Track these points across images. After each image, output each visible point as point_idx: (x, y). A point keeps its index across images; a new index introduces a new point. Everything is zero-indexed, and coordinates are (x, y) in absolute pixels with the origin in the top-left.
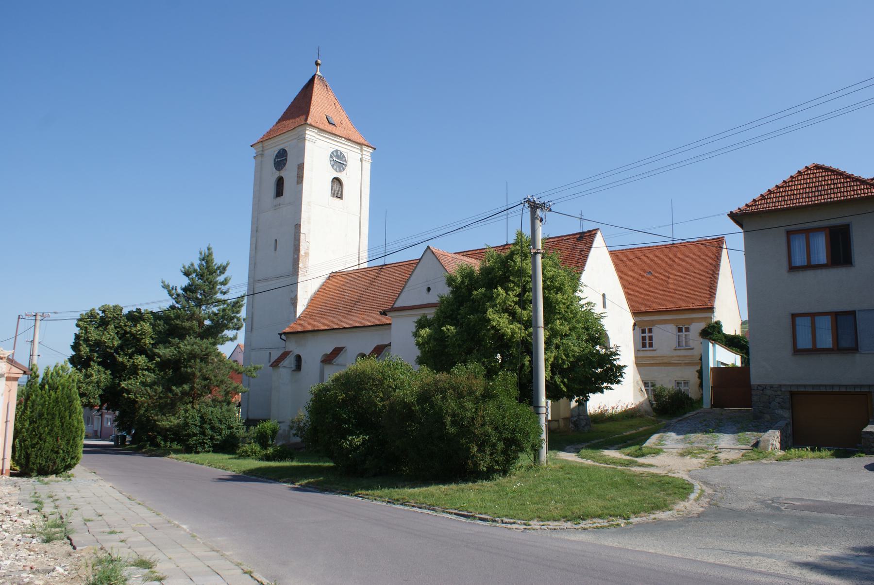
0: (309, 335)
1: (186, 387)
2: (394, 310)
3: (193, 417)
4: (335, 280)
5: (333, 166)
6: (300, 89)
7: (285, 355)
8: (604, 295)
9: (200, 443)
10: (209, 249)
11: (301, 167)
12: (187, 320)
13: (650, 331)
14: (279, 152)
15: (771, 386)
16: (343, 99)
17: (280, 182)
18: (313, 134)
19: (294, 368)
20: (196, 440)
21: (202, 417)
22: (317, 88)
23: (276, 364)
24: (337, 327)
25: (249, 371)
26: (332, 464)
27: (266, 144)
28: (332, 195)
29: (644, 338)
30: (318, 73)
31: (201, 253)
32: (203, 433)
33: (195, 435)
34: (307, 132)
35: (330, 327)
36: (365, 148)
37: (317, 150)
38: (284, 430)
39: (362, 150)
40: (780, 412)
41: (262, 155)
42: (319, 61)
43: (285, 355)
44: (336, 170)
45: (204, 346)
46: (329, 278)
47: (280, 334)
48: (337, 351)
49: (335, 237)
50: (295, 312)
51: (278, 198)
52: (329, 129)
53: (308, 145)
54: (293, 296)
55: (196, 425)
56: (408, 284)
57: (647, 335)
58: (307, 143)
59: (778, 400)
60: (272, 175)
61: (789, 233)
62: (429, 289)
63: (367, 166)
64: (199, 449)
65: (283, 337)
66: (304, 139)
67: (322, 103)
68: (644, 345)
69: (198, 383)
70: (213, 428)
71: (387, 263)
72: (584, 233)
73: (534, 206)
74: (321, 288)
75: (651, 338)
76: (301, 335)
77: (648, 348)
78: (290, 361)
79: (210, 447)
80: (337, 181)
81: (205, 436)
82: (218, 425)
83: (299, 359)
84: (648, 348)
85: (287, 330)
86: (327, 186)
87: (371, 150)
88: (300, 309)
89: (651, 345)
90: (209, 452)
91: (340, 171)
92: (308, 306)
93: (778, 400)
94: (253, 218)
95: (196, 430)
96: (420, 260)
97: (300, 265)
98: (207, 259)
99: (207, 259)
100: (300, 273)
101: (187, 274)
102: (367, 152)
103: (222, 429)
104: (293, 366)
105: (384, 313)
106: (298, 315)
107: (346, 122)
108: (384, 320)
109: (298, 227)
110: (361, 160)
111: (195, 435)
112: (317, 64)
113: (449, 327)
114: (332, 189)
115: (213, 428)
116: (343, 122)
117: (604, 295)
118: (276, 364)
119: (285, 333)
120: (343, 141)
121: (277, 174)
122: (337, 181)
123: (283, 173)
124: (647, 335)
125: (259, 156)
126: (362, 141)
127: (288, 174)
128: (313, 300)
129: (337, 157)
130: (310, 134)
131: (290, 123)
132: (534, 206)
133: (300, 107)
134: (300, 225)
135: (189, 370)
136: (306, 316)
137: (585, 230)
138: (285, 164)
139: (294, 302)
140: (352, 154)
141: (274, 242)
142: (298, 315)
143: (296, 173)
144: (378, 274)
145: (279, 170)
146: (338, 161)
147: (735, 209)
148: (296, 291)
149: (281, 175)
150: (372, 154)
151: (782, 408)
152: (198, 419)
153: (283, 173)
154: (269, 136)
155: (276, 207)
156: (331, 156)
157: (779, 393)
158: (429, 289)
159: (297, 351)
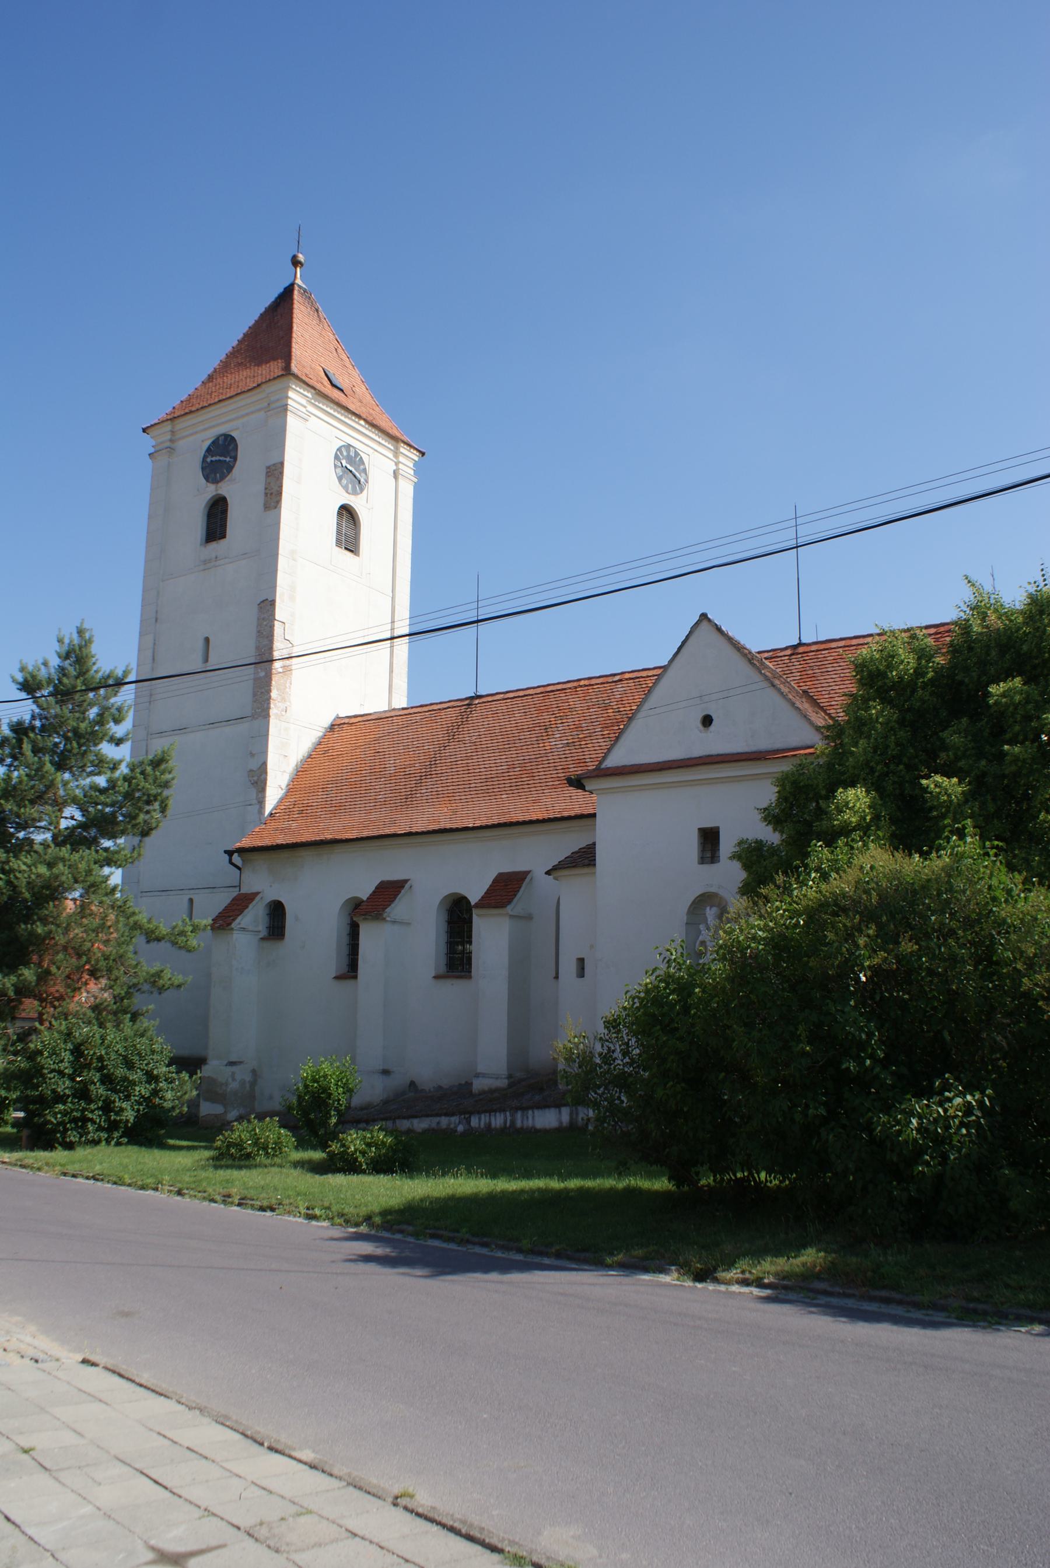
0: (304, 853)
1: (28, 974)
2: (602, 773)
3: (54, 1053)
4: (347, 732)
5: (340, 479)
6: (256, 316)
7: (241, 903)
9: (74, 1120)
10: (80, 632)
11: (275, 473)
12: (33, 802)
14: (215, 443)
16: (350, 340)
18: (304, 401)
19: (264, 933)
20: (65, 1113)
21: (77, 1051)
22: (301, 313)
23: (224, 921)
24: (387, 831)
25: (182, 933)
26: (662, 1184)
27: (180, 424)
28: (339, 543)
30: (299, 281)
31: (60, 641)
32: (83, 1093)
33: (60, 1099)
34: (291, 394)
35: (365, 834)
36: (403, 449)
37: (311, 439)
38: (243, 1083)
39: (396, 453)
41: (171, 450)
42: (301, 257)
43: (241, 903)
44: (346, 488)
45: (82, 866)
46: (332, 727)
47: (230, 853)
48: (389, 892)
49: (344, 639)
50: (261, 802)
51: (213, 545)
52: (331, 395)
53: (292, 422)
54: (254, 765)
55: (61, 1073)
56: (654, 699)
58: (291, 419)
60: (196, 494)
62: (707, 721)
63: (407, 489)
64: (73, 1136)
66: (285, 408)
67: (310, 340)
69: (61, 965)
70: (107, 1080)
71: (482, 692)
74: (314, 749)
76: (285, 854)
78: (254, 917)
79: (101, 1128)
80: (347, 512)
81: (90, 1101)
82: (120, 1072)
83: (277, 911)
85: (246, 842)
87: (415, 456)
88: (273, 795)
90: (96, 1142)
91: (355, 493)
92: (290, 790)
94: (145, 590)
95: (63, 1086)
97: (274, 694)
98: (77, 655)
99: (77, 655)
100: (273, 711)
101: (30, 686)
102: (408, 458)
103: (133, 1083)
104: (262, 928)
105: (577, 783)
106: (269, 807)
107: (361, 390)
108: (574, 802)
109: (267, 606)
110: (396, 474)
111: (60, 1099)
112: (296, 262)
113: (938, 778)
114: (339, 532)
115: (107, 1080)
116: (357, 389)
118: (224, 921)
119: (241, 851)
121: (211, 491)
122: (347, 512)
123: (225, 489)
126: (395, 432)
127: (240, 490)
128: (302, 772)
129: (349, 459)
130: (297, 398)
131: (246, 377)
133: (268, 342)
134: (273, 603)
135: (40, 930)
136: (288, 811)
139: (258, 780)
140: (380, 460)
141: (201, 643)
142: (269, 807)
143: (260, 487)
145: (216, 482)
146: (351, 470)
148: (265, 752)
149: (223, 495)
150: (416, 464)
152: (67, 1056)
153: (225, 489)
154: (189, 408)
156: (336, 457)
158: (707, 721)
159: (271, 893)
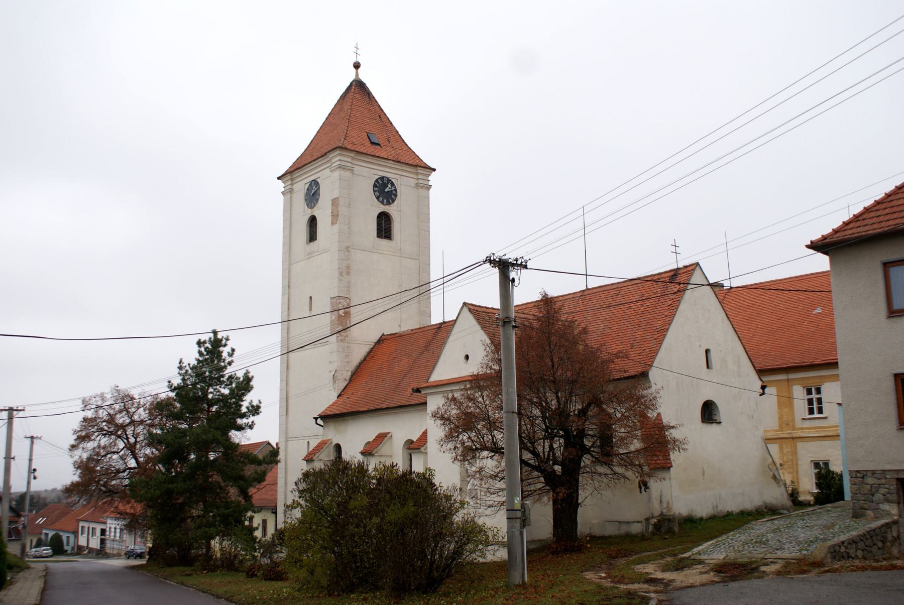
8: (707, 352)
13: (818, 391)
15: (873, 472)
17: (313, 221)
24: (379, 407)
29: (810, 402)
40: (886, 507)
44: (382, 202)
47: (316, 419)
48: (381, 438)
57: (814, 396)
59: (882, 491)
61: (886, 265)
62: (467, 357)
65: (320, 421)
68: (811, 411)
72: (678, 269)
73: (504, 266)
75: (820, 401)
77: (816, 415)
84: (816, 415)
86: (372, 226)
89: (820, 411)
91: (389, 203)
93: (882, 491)
96: (455, 321)
117: (707, 352)
120: (390, 164)
121: (309, 212)
123: (317, 212)
124: (814, 396)
125: (288, 192)
132: (504, 266)
137: (681, 266)
138: (317, 200)
144: (436, 334)
145: (312, 208)
147: (816, 236)
151: (889, 501)
155: (310, 255)
157: (883, 481)
158: (467, 357)
